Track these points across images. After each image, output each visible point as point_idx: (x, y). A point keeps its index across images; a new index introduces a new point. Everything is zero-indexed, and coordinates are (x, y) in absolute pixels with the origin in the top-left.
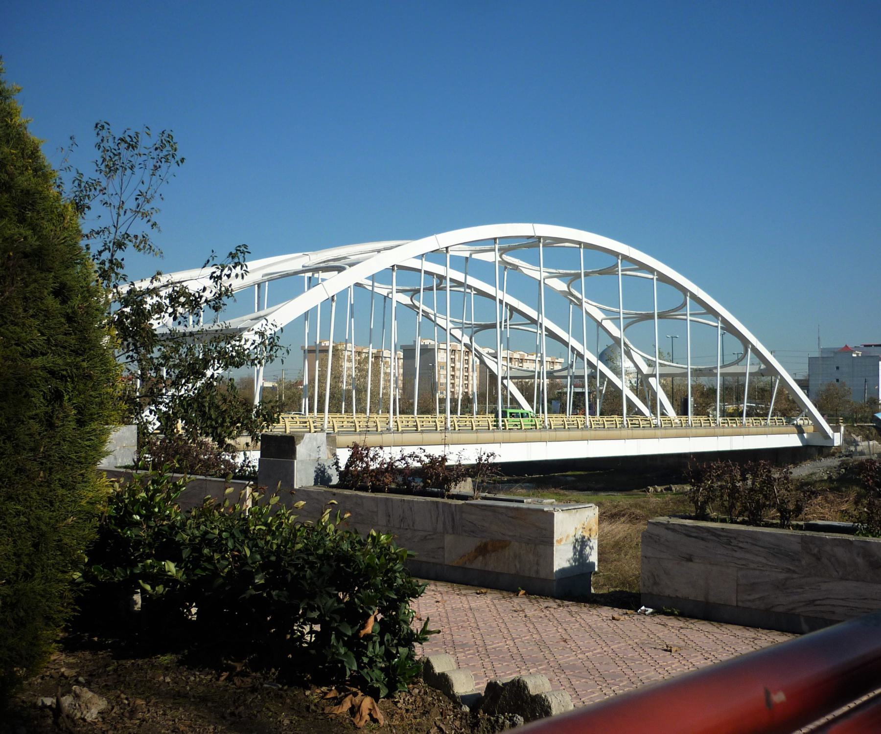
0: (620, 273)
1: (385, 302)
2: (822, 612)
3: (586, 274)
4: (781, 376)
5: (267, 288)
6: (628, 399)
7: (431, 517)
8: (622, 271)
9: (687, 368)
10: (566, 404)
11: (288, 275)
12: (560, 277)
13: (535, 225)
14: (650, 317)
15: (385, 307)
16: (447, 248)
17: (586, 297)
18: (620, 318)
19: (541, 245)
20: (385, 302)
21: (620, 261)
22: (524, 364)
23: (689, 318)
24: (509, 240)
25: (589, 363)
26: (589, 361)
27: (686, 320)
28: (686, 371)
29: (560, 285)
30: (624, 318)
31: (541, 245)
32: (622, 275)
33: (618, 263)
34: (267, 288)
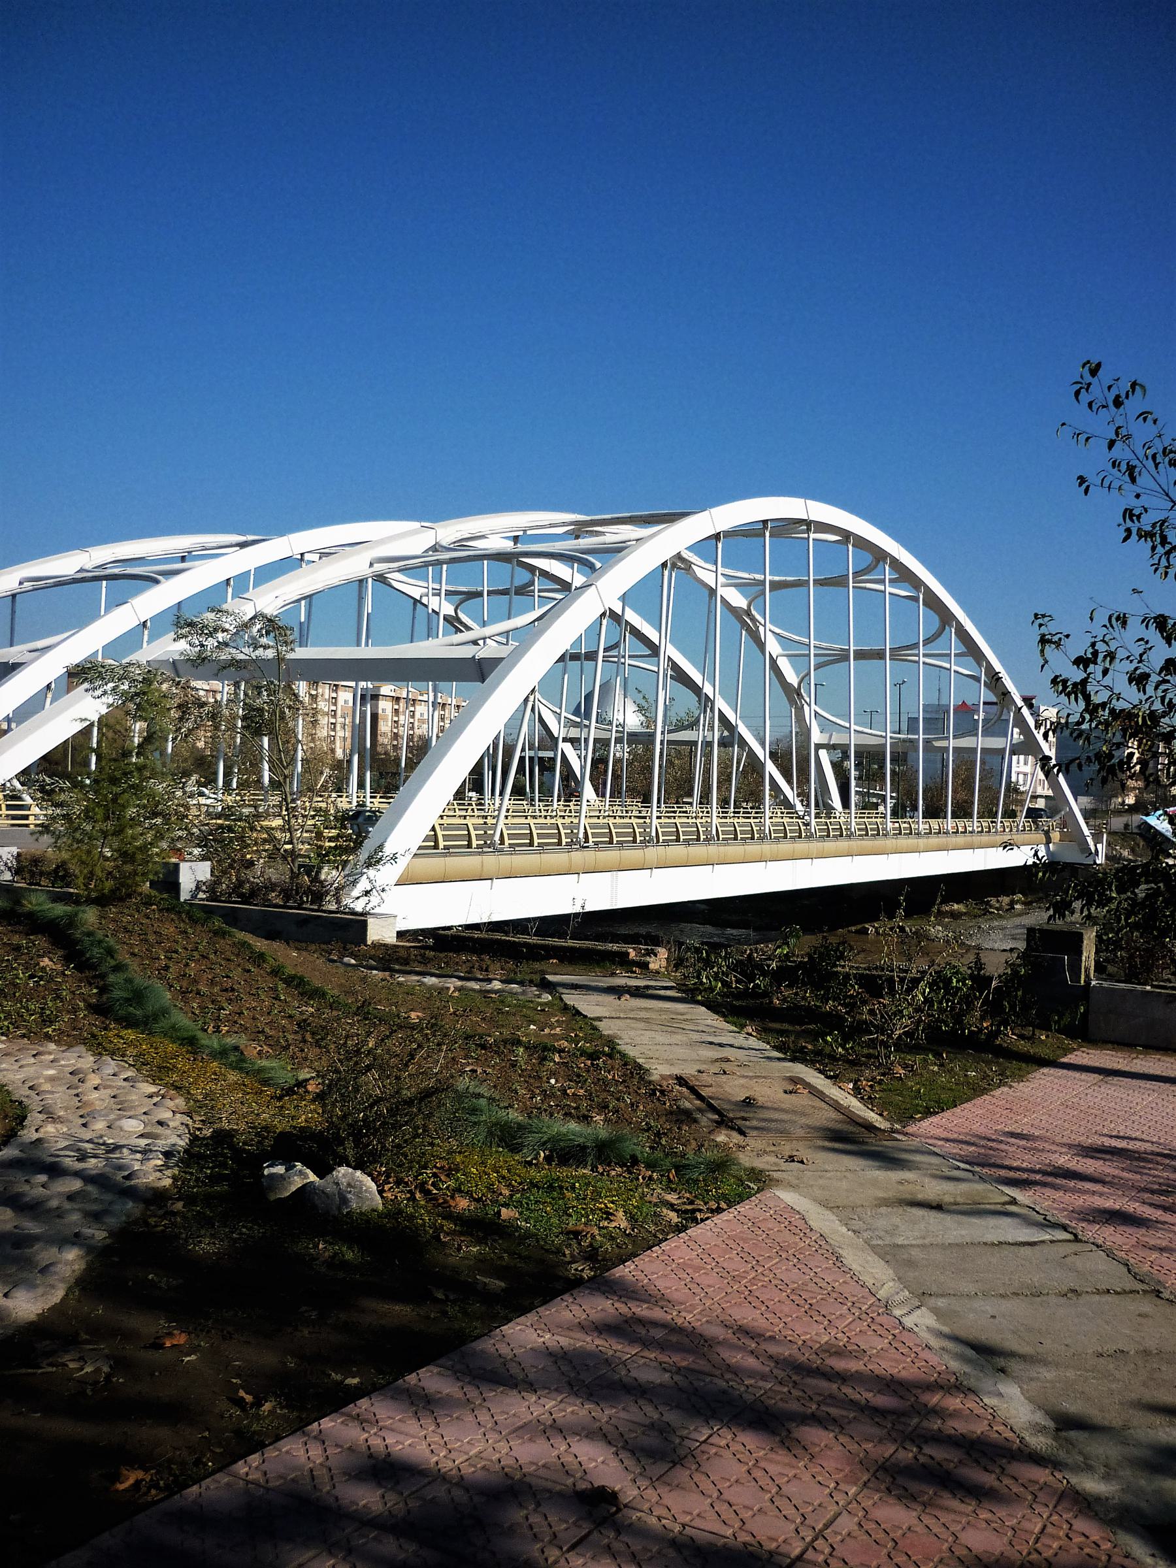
0: (536, 594)
1: (415, 609)
2: (1101, 1195)
3: (489, 593)
4: (750, 748)
5: (104, 590)
6: (772, 779)
7: (629, 977)
8: (540, 591)
9: (885, 737)
10: (694, 778)
11: (827, 541)
12: (740, 586)
13: (808, 502)
14: (880, 655)
15: (414, 618)
16: (302, 555)
17: (771, 622)
18: (809, 655)
19: (767, 534)
20: (415, 609)
21: (536, 579)
22: (417, 707)
23: (922, 659)
24: (138, 562)
25: (723, 718)
26: (722, 716)
27: (918, 662)
28: (882, 741)
29: (738, 600)
30: (815, 655)
31: (767, 534)
32: (539, 596)
33: (534, 581)
34: (104, 590)
